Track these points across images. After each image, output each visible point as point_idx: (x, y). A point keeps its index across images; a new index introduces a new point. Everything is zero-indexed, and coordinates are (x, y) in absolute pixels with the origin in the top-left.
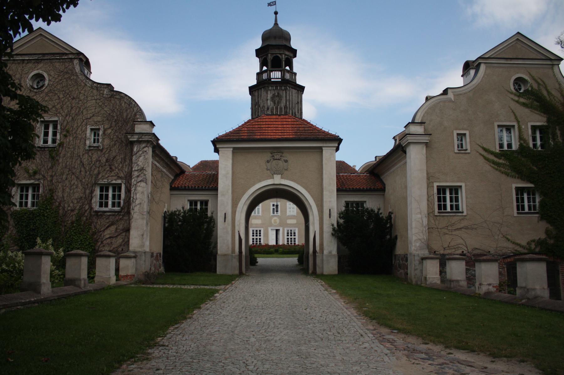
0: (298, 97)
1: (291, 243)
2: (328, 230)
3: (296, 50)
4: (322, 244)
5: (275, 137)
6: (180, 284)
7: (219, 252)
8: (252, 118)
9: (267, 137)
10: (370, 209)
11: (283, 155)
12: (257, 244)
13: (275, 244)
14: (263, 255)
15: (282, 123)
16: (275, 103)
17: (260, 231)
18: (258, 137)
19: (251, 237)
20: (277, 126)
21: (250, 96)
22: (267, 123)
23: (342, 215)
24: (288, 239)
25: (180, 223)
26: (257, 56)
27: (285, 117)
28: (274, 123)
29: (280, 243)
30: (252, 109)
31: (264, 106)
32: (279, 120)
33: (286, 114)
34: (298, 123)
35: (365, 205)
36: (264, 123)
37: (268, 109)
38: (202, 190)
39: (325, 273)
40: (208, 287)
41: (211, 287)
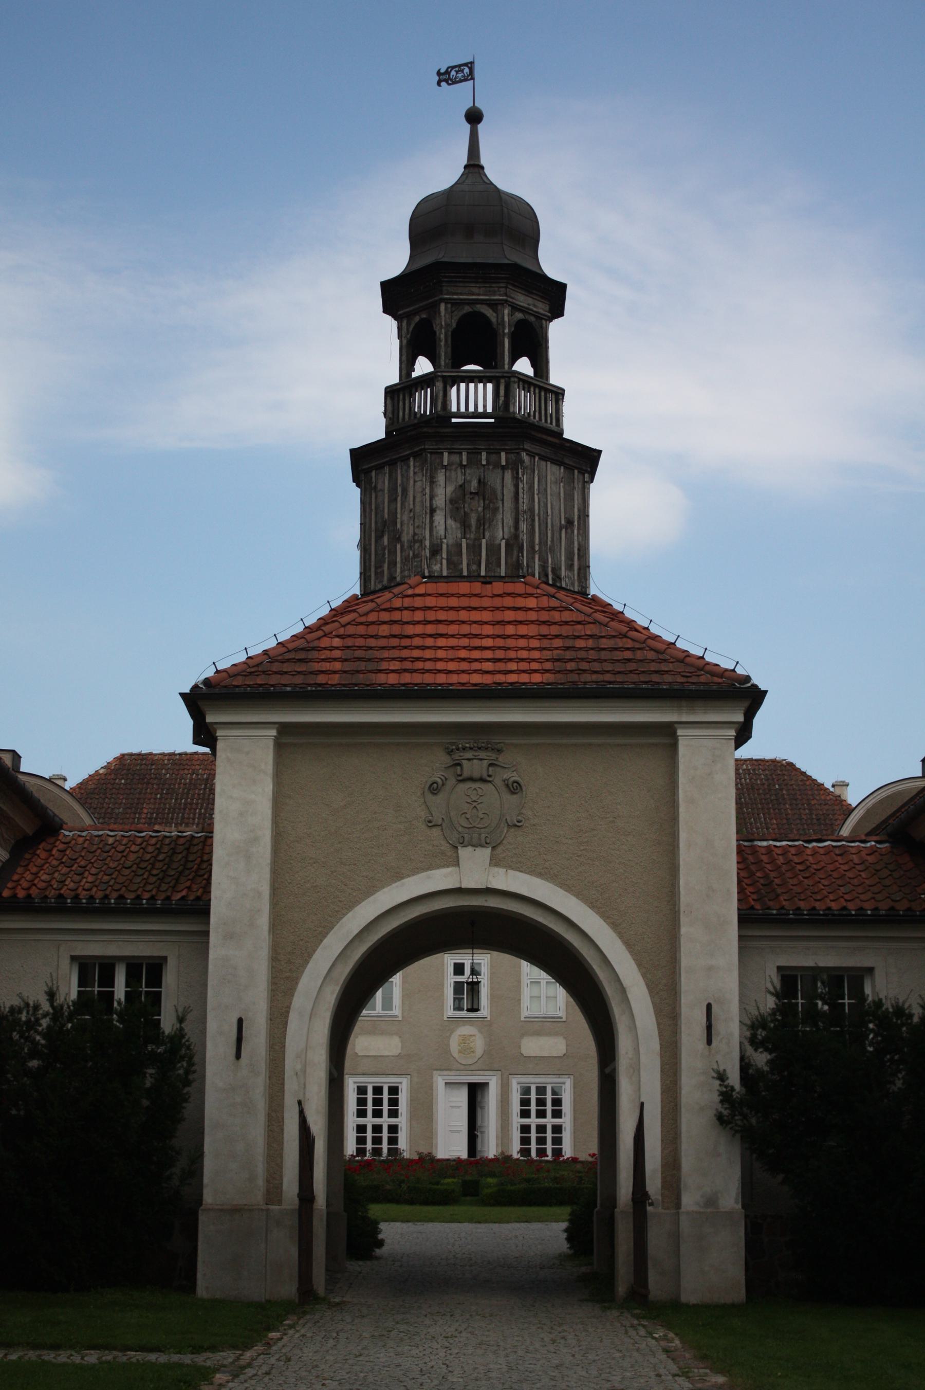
0: (569, 497)
1: (542, 1152)
2: (698, 1096)
3: (562, 287)
4: (672, 1164)
5: (464, 678)
6: (35, 1347)
7: (208, 1197)
8: (366, 590)
9: (428, 678)
10: (888, 1006)
11: (502, 759)
12: (377, 1152)
13: (464, 1155)
14: (407, 1208)
15: (499, 616)
16: (465, 526)
17: (394, 1090)
18: (392, 679)
19: (351, 1121)
20: (475, 629)
21: (358, 491)
22: (431, 616)
23: (759, 1032)
24: (525, 1129)
25: (34, 1063)
26: (386, 310)
27: (510, 588)
28: (463, 615)
29: (491, 1149)
30: (364, 546)
31: (417, 540)
32: (486, 602)
33: (516, 573)
34: (566, 616)
35: (868, 990)
36: (419, 616)
37: (435, 551)
38: (136, 911)
39: (689, 1296)
40: (163, 1358)
41: (175, 1358)
